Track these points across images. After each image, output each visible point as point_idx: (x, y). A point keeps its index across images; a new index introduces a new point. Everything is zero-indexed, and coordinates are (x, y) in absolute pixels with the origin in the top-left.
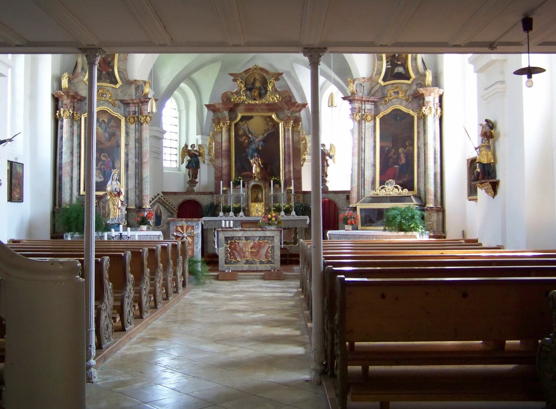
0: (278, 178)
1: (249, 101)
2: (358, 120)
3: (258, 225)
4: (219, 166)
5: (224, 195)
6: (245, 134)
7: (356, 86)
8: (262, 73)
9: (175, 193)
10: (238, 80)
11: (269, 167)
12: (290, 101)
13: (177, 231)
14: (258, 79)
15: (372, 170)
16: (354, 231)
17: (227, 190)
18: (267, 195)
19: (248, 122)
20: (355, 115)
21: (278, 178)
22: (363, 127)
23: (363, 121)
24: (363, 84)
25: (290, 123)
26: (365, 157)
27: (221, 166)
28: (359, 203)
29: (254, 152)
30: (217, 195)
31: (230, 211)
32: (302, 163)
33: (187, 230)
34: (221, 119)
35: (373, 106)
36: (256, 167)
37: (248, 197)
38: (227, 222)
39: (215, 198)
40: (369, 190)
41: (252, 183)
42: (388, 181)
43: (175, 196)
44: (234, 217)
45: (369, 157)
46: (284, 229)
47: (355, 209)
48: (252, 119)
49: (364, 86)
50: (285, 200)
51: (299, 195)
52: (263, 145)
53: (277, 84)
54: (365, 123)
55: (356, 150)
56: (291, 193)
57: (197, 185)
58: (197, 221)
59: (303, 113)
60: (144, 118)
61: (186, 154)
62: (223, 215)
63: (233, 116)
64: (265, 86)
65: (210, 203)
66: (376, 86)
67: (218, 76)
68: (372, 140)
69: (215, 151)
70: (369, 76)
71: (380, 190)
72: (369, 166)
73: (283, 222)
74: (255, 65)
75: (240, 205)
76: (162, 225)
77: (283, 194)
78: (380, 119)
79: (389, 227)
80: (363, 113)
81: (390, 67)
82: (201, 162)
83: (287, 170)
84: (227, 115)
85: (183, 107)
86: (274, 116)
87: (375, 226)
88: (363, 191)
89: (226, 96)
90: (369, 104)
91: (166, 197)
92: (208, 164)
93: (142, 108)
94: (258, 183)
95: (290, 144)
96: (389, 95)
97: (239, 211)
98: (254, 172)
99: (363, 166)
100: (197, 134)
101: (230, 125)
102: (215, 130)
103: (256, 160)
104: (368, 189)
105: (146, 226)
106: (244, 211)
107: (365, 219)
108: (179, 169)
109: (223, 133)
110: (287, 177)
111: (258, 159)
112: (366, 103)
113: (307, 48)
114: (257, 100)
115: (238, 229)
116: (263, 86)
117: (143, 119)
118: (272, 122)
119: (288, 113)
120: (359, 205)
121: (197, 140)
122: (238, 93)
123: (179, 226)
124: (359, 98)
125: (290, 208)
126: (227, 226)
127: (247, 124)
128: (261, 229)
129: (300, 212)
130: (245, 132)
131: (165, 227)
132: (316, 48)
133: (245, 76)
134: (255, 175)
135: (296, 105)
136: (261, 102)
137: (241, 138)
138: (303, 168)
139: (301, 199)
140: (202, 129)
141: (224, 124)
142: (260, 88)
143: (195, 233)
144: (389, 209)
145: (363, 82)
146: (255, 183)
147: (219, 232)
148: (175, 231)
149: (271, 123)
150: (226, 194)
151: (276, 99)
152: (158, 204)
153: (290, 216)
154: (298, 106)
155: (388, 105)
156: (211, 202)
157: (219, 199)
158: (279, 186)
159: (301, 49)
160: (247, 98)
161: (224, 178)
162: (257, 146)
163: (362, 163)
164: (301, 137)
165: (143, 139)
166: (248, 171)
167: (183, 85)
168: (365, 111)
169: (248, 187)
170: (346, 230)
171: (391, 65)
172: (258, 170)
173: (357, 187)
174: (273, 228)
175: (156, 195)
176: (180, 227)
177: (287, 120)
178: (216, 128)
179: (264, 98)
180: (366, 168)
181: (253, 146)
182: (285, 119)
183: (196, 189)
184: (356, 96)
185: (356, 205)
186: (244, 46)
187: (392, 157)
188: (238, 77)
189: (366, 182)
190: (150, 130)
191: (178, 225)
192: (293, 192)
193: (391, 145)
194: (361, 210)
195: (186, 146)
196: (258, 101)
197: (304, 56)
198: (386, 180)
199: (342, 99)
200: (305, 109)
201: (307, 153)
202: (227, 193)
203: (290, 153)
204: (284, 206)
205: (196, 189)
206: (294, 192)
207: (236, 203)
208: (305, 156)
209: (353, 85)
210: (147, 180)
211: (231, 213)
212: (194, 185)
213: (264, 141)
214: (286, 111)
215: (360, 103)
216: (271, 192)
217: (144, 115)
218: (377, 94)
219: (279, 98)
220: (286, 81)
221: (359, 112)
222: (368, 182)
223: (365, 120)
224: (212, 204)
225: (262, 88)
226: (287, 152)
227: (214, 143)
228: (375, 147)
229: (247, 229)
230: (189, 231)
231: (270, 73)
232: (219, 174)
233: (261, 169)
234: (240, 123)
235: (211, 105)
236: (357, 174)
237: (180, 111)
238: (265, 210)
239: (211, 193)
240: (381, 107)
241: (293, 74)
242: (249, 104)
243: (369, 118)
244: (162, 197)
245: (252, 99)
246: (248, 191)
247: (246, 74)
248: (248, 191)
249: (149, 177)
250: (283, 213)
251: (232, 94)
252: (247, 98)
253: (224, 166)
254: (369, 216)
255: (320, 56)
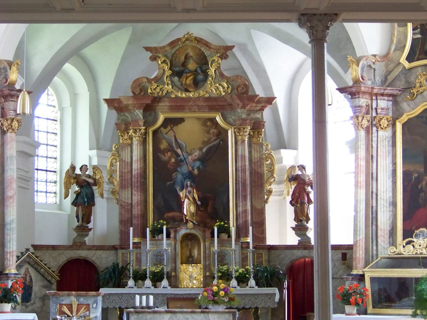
0: (225, 223)
1: (176, 93)
2: (365, 126)
3: (196, 302)
4: (126, 201)
5: (136, 251)
6: (170, 149)
7: (363, 69)
8: (199, 46)
9: (54, 248)
10: (160, 57)
11: (210, 203)
12: (247, 92)
13: (62, 313)
14: (191, 56)
15: (389, 211)
16: (362, 316)
17: (140, 243)
18: (207, 252)
19: (175, 128)
20: (360, 119)
21: (225, 223)
22: (375, 139)
23: (374, 129)
24: (373, 66)
25: (245, 130)
26: (377, 189)
27: (130, 202)
28: (368, 268)
29: (185, 179)
30: (124, 251)
31: (146, 278)
32: (266, 197)
33: (78, 311)
34: (130, 123)
35: (391, 103)
36: (189, 204)
37: (175, 255)
38: (144, 297)
39: (120, 255)
40: (385, 246)
41: (183, 231)
42: (418, 231)
43: (53, 251)
44: (153, 288)
45: (385, 190)
46: (239, 310)
47: (361, 278)
48: (183, 123)
49: (374, 70)
50: (237, 260)
51: (261, 251)
52: (201, 167)
53: (224, 64)
54: (377, 131)
55: (362, 178)
56: (249, 248)
57: (91, 233)
58: (94, 296)
59: (267, 114)
60: (9, 122)
61: (72, 181)
62: (133, 286)
63: (150, 119)
64: (204, 68)
65: (111, 264)
66: (395, 70)
67: (126, 51)
68: (389, 160)
69: (121, 176)
70: (384, 52)
71: (404, 247)
72: (385, 205)
73: (237, 299)
74: (188, 33)
75: (163, 269)
76: (32, 302)
77: (235, 251)
78: (404, 125)
79: (422, 309)
80: (374, 114)
81: (419, 36)
82: (97, 195)
83: (241, 210)
84: (141, 117)
85: (67, 103)
86: (219, 119)
87: (394, 307)
88: (375, 248)
89: (140, 85)
90: (384, 100)
91: (39, 253)
92: (107, 198)
93: (4, 106)
94: (193, 231)
95: (245, 165)
96: (418, 85)
97: (160, 279)
98: (185, 213)
99: (374, 205)
100: (90, 149)
101: (146, 134)
102: (121, 141)
103: (190, 192)
104: (382, 244)
105: (10, 304)
106: (169, 278)
107: (379, 295)
108: (60, 207)
109: (135, 147)
110: (241, 221)
111: (192, 191)
112: (379, 98)
113: (306, 14)
114: (190, 92)
115: (160, 309)
116: (201, 68)
117: (6, 124)
118: (216, 128)
119: (242, 113)
120: (368, 271)
121: (90, 158)
122: (158, 80)
123: (65, 305)
124: (367, 89)
125: (246, 274)
126: (144, 304)
127: (174, 132)
128: (200, 310)
129: (263, 281)
130: (170, 145)
131: (38, 304)
132: (321, 15)
133: (170, 52)
134: (187, 218)
135: (256, 100)
136: (196, 95)
137: (164, 155)
138: (267, 206)
139: (265, 257)
140: (98, 140)
141: (135, 132)
142: (196, 71)
143: (92, 316)
144: (422, 278)
145: (374, 63)
146: (188, 231)
147: (130, 315)
148: (58, 313)
149: (213, 131)
150: (138, 250)
151: (222, 89)
152: (27, 266)
153: (247, 288)
154: (259, 102)
155: (417, 100)
156: (113, 263)
157: (127, 257)
158: (227, 236)
159: (296, 15)
160: (174, 87)
161: (135, 221)
162: (190, 169)
163: (372, 199)
164: (265, 154)
165: (5, 158)
166: (174, 211)
167: (68, 67)
168: (376, 112)
169: (175, 238)
170: (347, 315)
171: (421, 33)
172: (193, 209)
173: (364, 241)
174: (221, 308)
175: (24, 250)
176: (66, 305)
177: (241, 125)
178: (121, 138)
179: (202, 88)
180: (379, 208)
181: (184, 169)
182: (238, 122)
183: (88, 240)
184: (362, 85)
185: (363, 271)
186: (203, 11)
187: (424, 189)
188: (159, 52)
189: (379, 231)
190: (17, 141)
191: (64, 303)
192: (251, 247)
193: (422, 170)
194: (373, 279)
195: (73, 168)
196: (193, 93)
197: (300, 26)
198: (413, 228)
199: (338, 91)
200: (270, 106)
201: (274, 180)
202: (140, 248)
203: (245, 180)
204: (237, 271)
205: (88, 240)
206: (254, 248)
207: (155, 265)
208: (270, 185)
209: (356, 67)
210: (12, 226)
211: (148, 282)
212: (85, 233)
213: (203, 159)
214: (239, 110)
215: (369, 98)
216: (214, 247)
217: (9, 117)
218: (398, 83)
219: (228, 88)
220: (239, 62)
221: (367, 113)
222: (383, 232)
223: (379, 126)
224: (115, 266)
225: (199, 70)
226: (240, 180)
227: (118, 163)
228: (394, 172)
229: (177, 310)
230: (82, 311)
231: (213, 46)
232: (127, 216)
233: (198, 207)
234: (162, 129)
235: (114, 99)
236: (364, 218)
237: (62, 109)
238: (205, 277)
239: (114, 248)
240: (405, 105)
241: (250, 48)
242: (177, 97)
243: (384, 123)
244: (33, 253)
245: (181, 90)
246: (175, 244)
247: (172, 48)
248: (175, 244)
249: (15, 221)
250: (234, 282)
251: (149, 81)
252: (174, 87)
253: (136, 201)
254: (385, 289)
255: (328, 28)
